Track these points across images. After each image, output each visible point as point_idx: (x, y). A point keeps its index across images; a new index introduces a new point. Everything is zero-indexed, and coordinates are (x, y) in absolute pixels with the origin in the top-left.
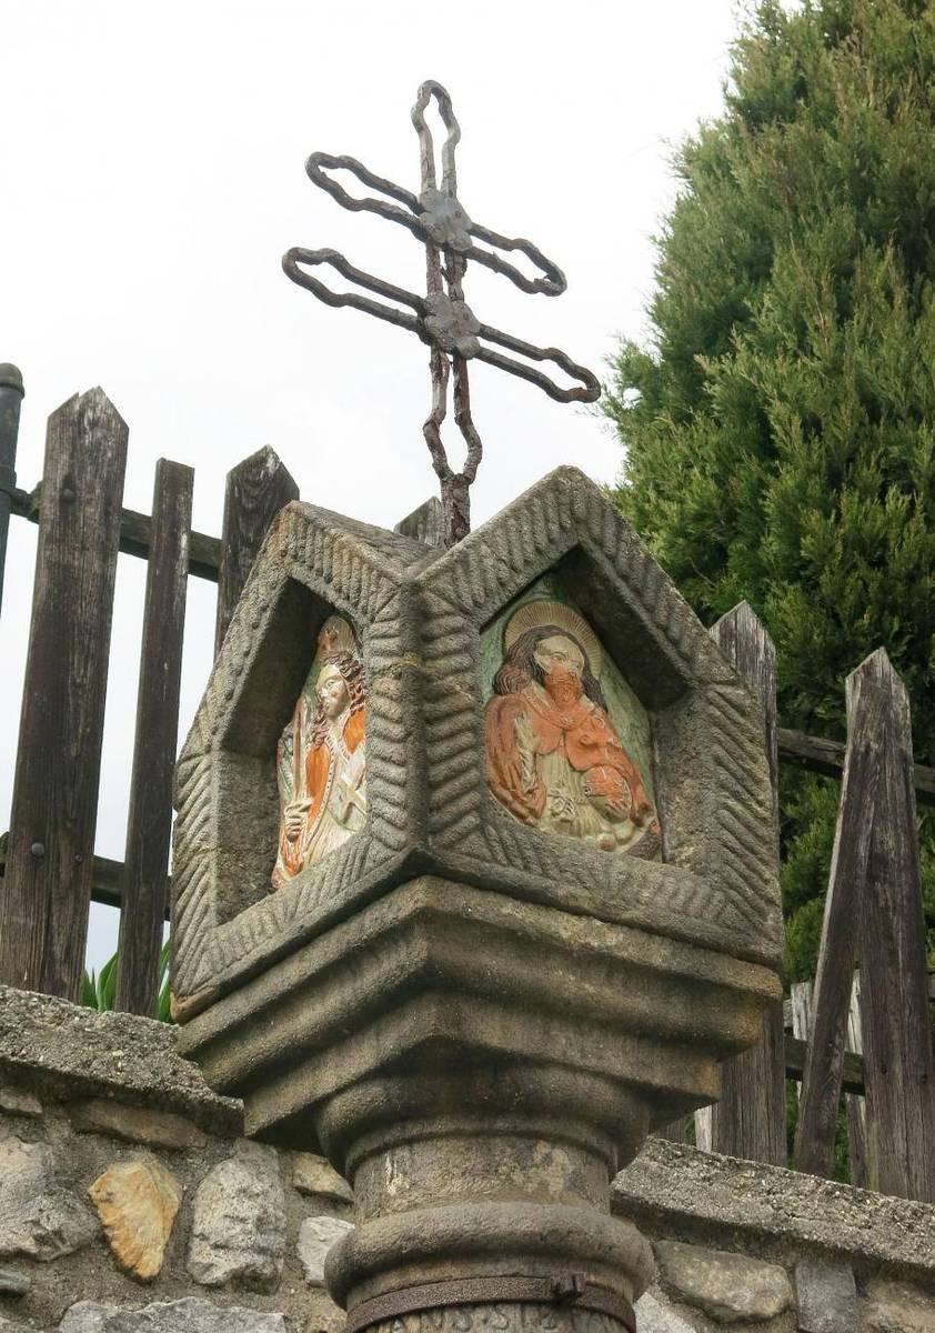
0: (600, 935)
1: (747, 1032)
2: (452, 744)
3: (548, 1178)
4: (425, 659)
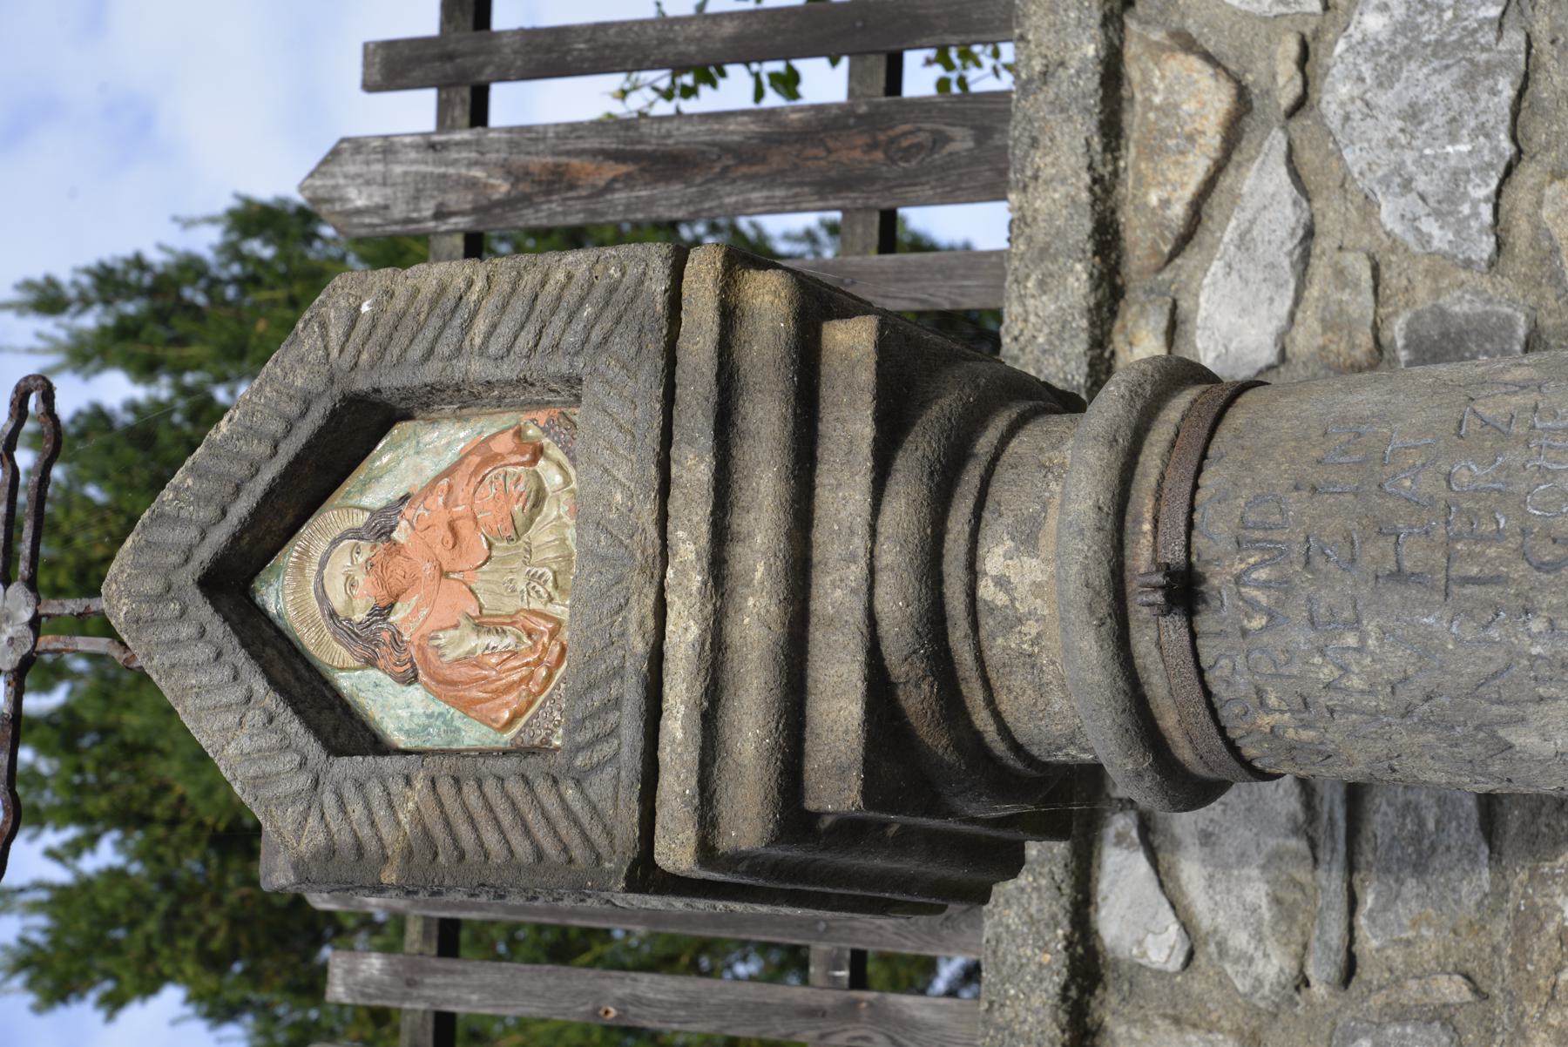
0: (682, 573)
1: (776, 294)
2: (483, 823)
3: (1027, 582)
4: (385, 858)
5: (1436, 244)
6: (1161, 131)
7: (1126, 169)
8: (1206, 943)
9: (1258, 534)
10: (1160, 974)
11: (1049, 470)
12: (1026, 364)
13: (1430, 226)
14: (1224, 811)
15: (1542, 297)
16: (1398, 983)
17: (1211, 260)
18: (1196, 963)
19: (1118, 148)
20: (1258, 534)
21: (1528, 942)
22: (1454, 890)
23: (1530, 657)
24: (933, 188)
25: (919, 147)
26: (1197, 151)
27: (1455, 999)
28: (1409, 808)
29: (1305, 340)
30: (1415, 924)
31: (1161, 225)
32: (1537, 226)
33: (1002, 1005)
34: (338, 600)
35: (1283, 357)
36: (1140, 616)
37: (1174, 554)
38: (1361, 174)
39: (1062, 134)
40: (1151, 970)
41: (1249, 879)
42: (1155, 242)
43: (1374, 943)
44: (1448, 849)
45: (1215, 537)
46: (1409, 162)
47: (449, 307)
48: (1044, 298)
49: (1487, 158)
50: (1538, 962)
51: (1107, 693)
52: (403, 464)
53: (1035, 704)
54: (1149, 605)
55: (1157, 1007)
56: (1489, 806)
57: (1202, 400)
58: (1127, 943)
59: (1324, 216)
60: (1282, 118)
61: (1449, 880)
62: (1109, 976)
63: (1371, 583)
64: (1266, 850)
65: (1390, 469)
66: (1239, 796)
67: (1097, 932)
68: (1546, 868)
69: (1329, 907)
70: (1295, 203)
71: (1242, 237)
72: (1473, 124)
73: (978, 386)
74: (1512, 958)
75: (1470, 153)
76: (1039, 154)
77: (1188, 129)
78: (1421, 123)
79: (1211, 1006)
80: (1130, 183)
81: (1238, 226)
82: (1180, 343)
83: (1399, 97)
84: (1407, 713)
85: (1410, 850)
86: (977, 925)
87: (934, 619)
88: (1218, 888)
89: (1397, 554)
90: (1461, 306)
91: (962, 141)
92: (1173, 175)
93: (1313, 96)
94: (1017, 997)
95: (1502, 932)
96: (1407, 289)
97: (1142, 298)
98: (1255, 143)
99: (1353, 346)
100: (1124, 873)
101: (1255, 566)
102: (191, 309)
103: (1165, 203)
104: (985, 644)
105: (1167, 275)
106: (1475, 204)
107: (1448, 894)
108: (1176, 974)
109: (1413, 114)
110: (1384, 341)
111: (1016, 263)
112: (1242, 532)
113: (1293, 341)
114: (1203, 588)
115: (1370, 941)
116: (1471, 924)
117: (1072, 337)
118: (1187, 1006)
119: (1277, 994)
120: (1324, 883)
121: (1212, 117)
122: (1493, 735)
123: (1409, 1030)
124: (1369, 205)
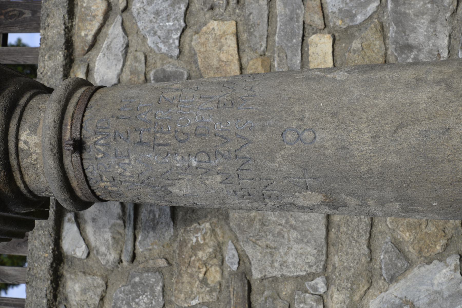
3: (33, 143)
5: (163, 51)
6: (85, 14)
7: (75, 25)
8: (93, 250)
9: (101, 130)
10: (80, 259)
11: (41, 110)
12: (44, 81)
13: (161, 45)
14: (99, 212)
15: (191, 67)
16: (147, 261)
17: (99, 52)
18: (90, 256)
19: (73, 19)
20: (101, 130)
21: (183, 249)
22: (163, 235)
23: (177, 167)
24: (19, 28)
25: (15, 15)
26: (96, 20)
27: (163, 266)
28: (151, 211)
29: (125, 77)
30: (152, 244)
31: (85, 42)
32: (191, 47)
33: (33, 269)
35: (119, 81)
36: (66, 153)
37: (76, 135)
38: (142, 29)
39: (56, 13)
40: (77, 258)
41: (106, 232)
42: (83, 47)
43: (141, 250)
44: (162, 223)
46: (156, 27)
48: (50, 61)
49: (177, 27)
51: (56, 176)
53: (35, 179)
54: (68, 150)
55: (79, 269)
56: (174, 210)
57: (87, 91)
58: (70, 250)
59: (132, 41)
60: (120, 12)
61: (162, 232)
62: (65, 260)
63: (133, 145)
64: (111, 223)
65: (139, 112)
66: (104, 208)
67: (62, 247)
68: (188, 228)
69: (128, 240)
70: (124, 37)
71: (108, 46)
72: (173, 17)
73: (21, 84)
74: (179, 254)
75: (173, 25)
76: (49, 19)
77: (93, 14)
78: (159, 16)
79: (94, 268)
80: (76, 29)
81: (107, 43)
82: (90, 76)
83: (153, 8)
84: (142, 183)
85: (151, 223)
86: (27, 246)
88: (97, 234)
89: (140, 137)
90: (169, 69)
92: (89, 27)
93: (130, 7)
94: (38, 266)
95: (176, 246)
96: (154, 63)
97: (79, 63)
98: (113, 19)
99: (139, 79)
100: (70, 230)
101: (100, 139)
103: (86, 35)
104: (21, 161)
105: (86, 56)
106: (174, 40)
107: (162, 236)
108: (84, 259)
109: (157, 13)
110: (148, 78)
111: (42, 51)
112: (96, 129)
113: (122, 77)
114: (85, 145)
115: (140, 249)
116: (168, 244)
117: (58, 73)
118: (87, 268)
119: (113, 265)
120: (127, 233)
121: (100, 11)
122: (166, 189)
123: (150, 274)
124: (144, 39)
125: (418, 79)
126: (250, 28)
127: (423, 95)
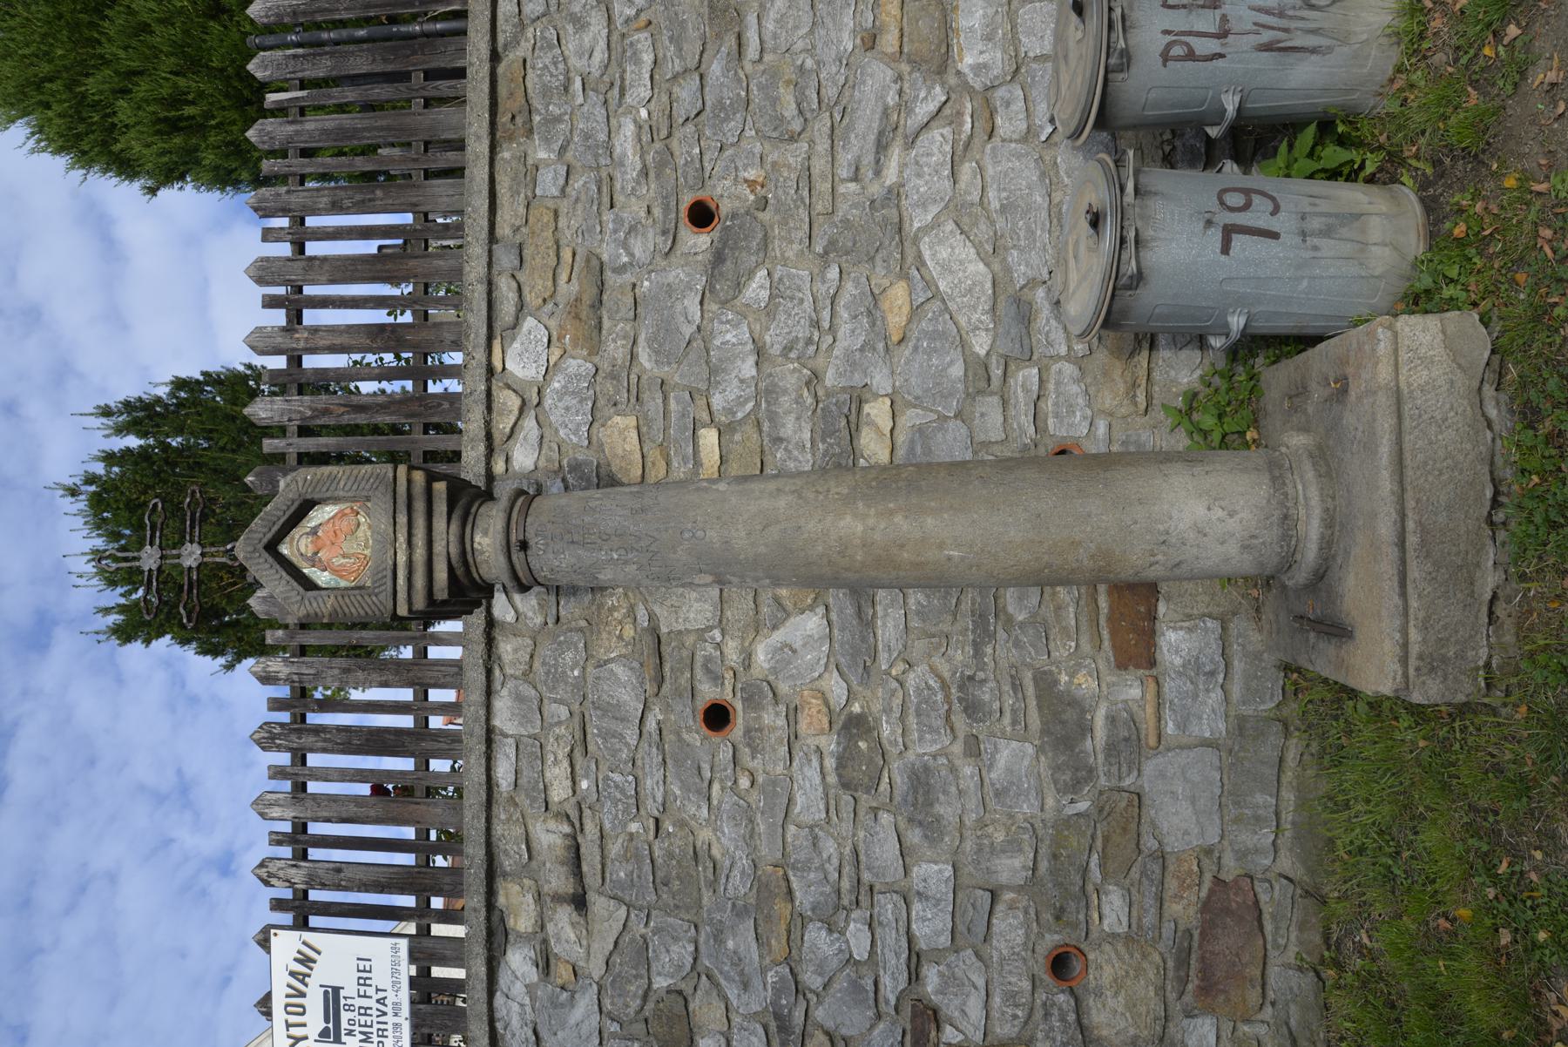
29: (542, 464)
34: (303, 550)
45: (530, 534)
47: (333, 479)
50: (603, 616)
52: (319, 516)
87: (463, 553)
90: (580, 457)
91: (446, 405)
102: (158, 414)
109: (567, 409)
115: (562, 613)
124: (557, 431)
125: (778, 490)
126: (650, 423)
127: (782, 503)
